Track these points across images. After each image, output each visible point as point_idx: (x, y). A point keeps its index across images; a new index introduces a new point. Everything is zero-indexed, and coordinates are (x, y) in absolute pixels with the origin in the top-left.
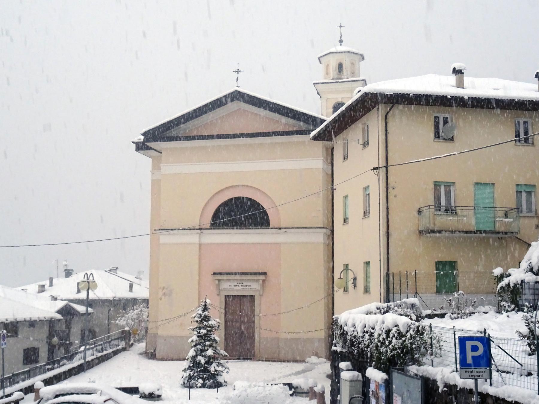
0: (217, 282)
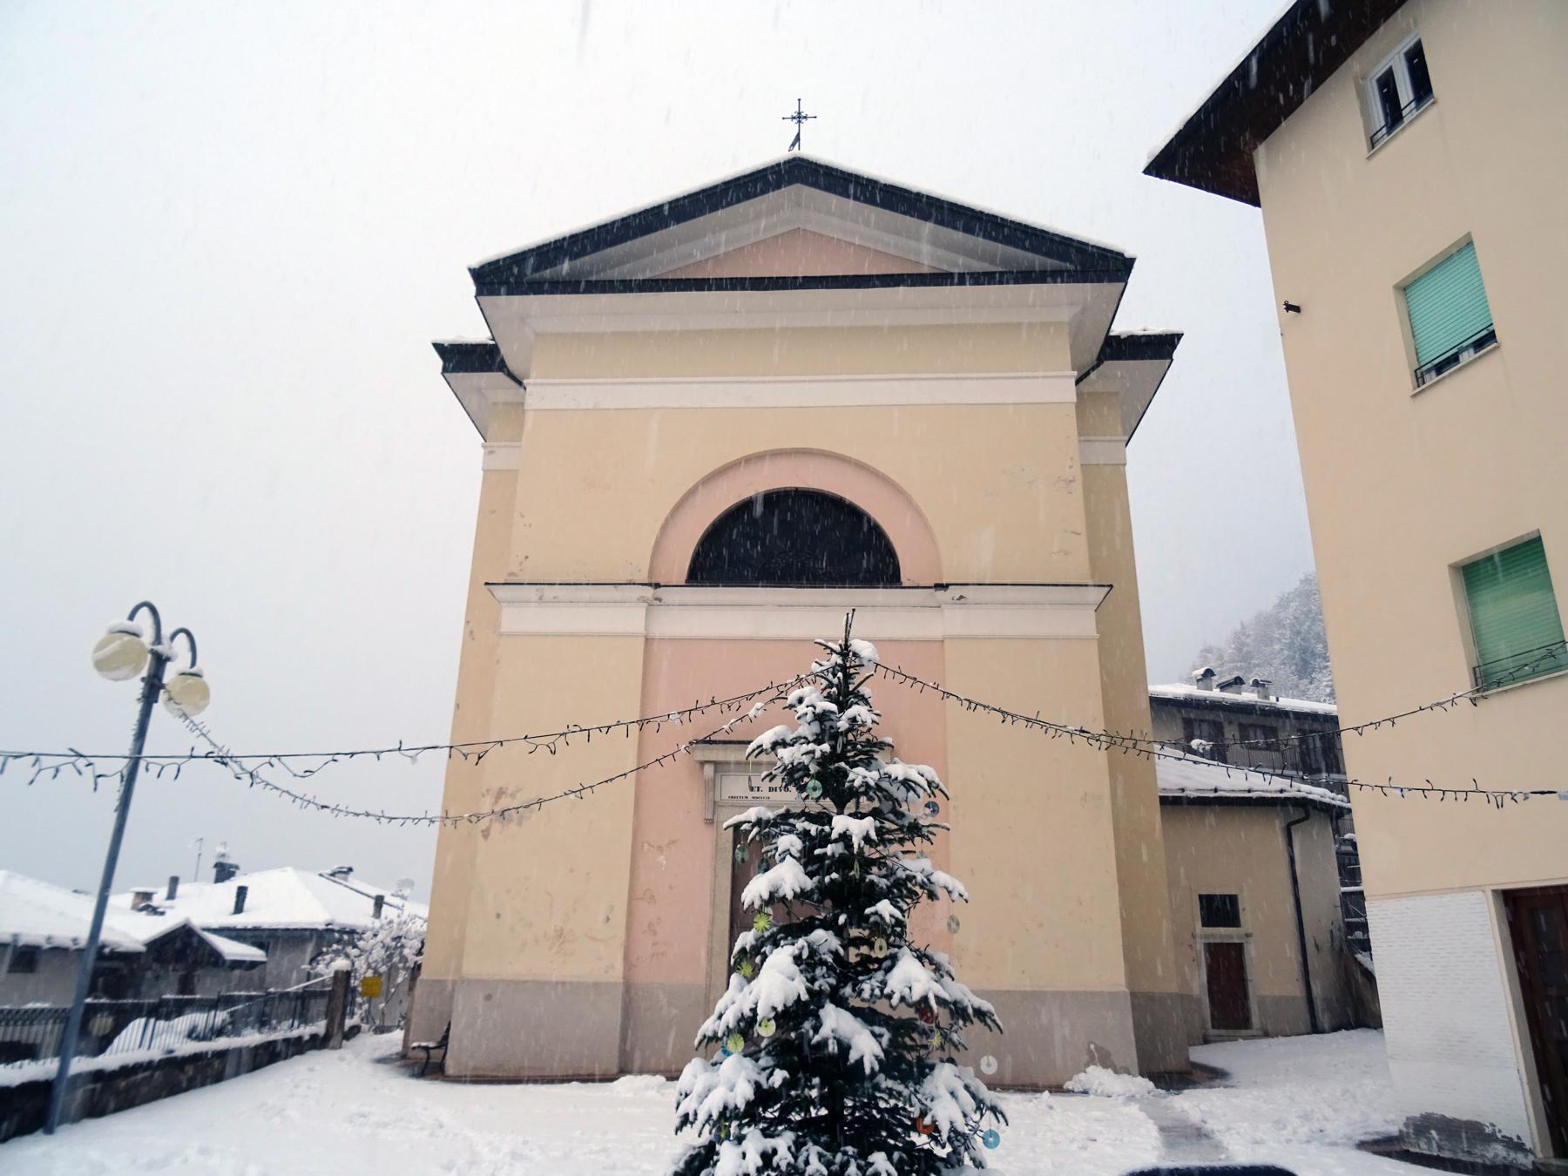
0: (709, 769)
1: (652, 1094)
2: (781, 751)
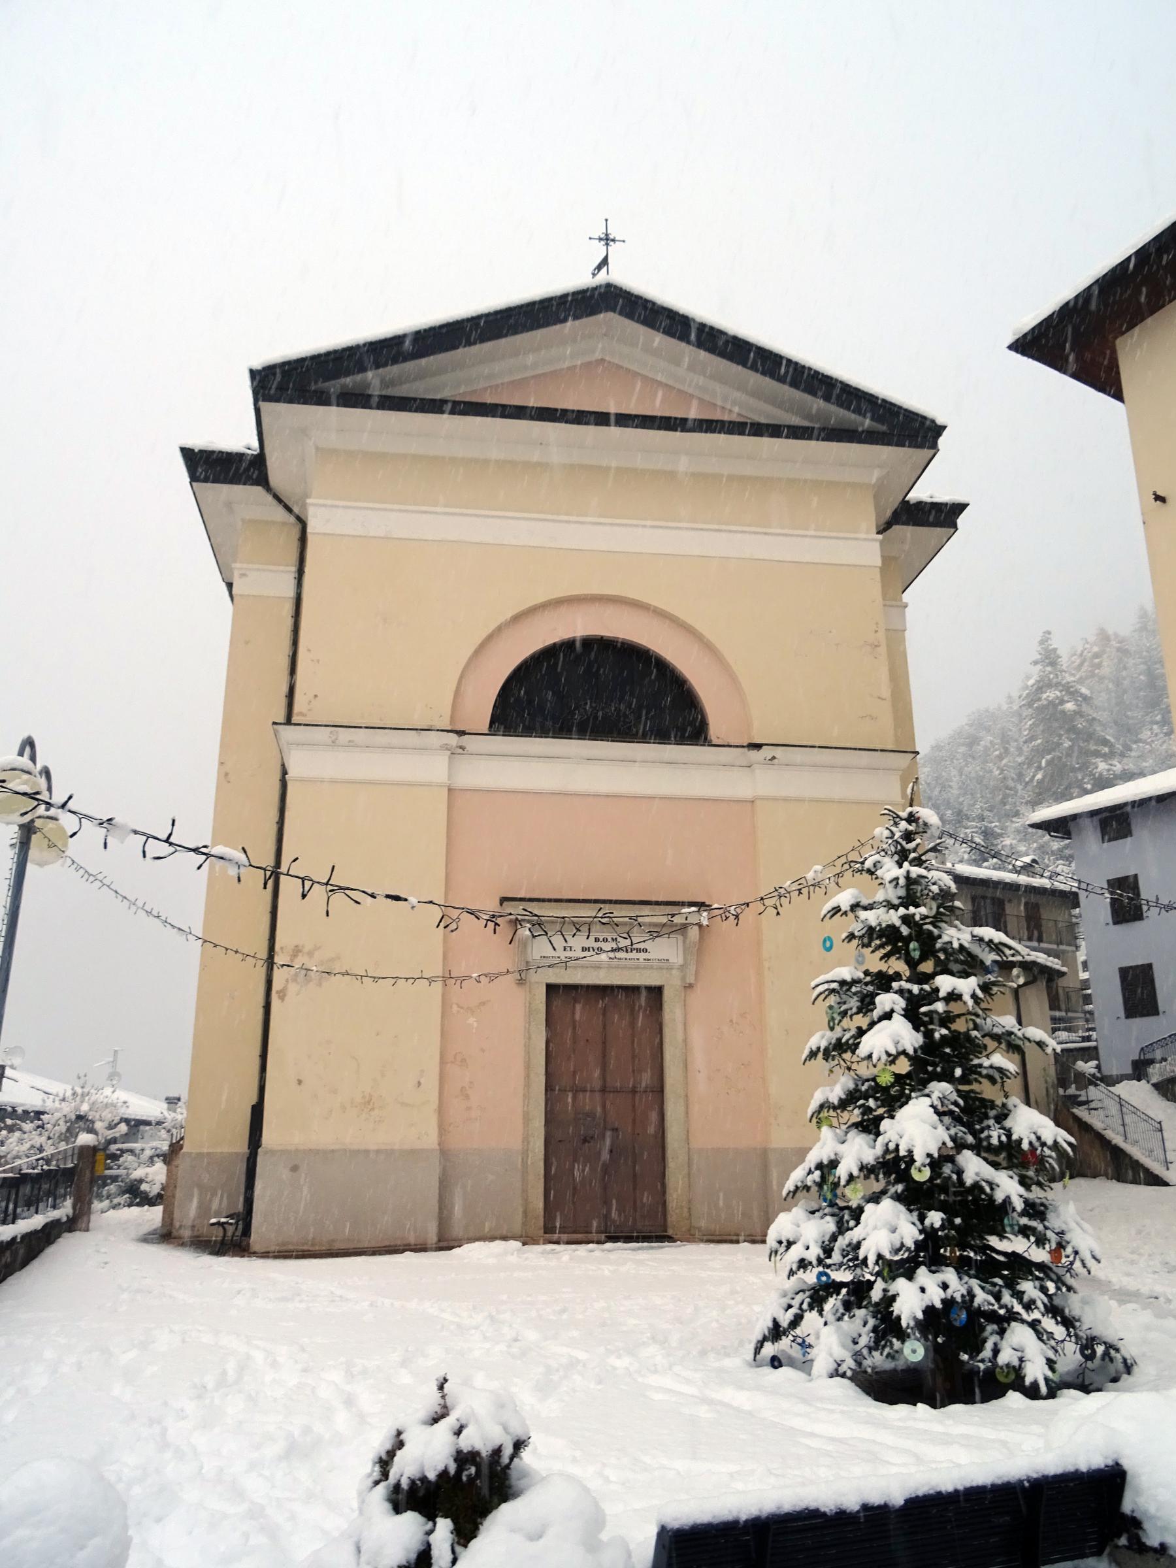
1: (513, 1259)
2: (863, 915)
